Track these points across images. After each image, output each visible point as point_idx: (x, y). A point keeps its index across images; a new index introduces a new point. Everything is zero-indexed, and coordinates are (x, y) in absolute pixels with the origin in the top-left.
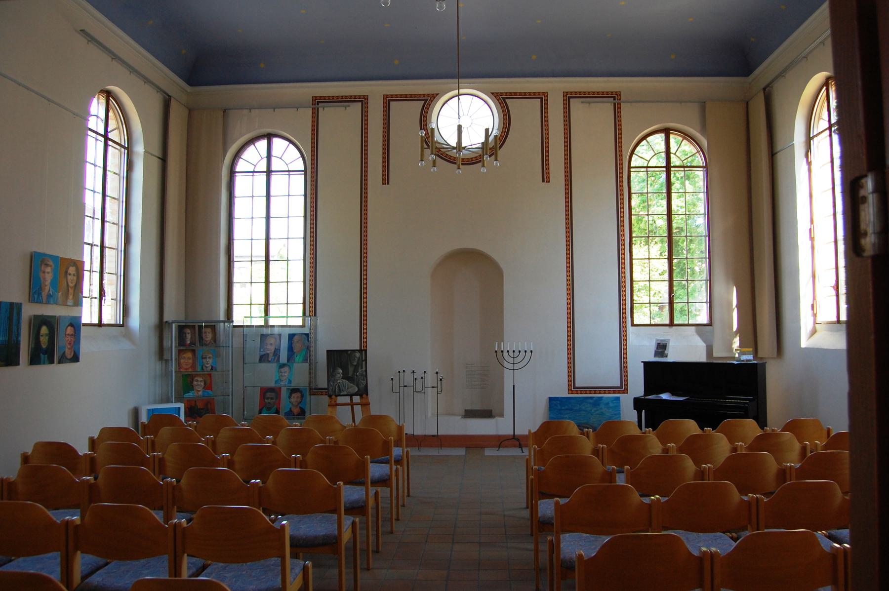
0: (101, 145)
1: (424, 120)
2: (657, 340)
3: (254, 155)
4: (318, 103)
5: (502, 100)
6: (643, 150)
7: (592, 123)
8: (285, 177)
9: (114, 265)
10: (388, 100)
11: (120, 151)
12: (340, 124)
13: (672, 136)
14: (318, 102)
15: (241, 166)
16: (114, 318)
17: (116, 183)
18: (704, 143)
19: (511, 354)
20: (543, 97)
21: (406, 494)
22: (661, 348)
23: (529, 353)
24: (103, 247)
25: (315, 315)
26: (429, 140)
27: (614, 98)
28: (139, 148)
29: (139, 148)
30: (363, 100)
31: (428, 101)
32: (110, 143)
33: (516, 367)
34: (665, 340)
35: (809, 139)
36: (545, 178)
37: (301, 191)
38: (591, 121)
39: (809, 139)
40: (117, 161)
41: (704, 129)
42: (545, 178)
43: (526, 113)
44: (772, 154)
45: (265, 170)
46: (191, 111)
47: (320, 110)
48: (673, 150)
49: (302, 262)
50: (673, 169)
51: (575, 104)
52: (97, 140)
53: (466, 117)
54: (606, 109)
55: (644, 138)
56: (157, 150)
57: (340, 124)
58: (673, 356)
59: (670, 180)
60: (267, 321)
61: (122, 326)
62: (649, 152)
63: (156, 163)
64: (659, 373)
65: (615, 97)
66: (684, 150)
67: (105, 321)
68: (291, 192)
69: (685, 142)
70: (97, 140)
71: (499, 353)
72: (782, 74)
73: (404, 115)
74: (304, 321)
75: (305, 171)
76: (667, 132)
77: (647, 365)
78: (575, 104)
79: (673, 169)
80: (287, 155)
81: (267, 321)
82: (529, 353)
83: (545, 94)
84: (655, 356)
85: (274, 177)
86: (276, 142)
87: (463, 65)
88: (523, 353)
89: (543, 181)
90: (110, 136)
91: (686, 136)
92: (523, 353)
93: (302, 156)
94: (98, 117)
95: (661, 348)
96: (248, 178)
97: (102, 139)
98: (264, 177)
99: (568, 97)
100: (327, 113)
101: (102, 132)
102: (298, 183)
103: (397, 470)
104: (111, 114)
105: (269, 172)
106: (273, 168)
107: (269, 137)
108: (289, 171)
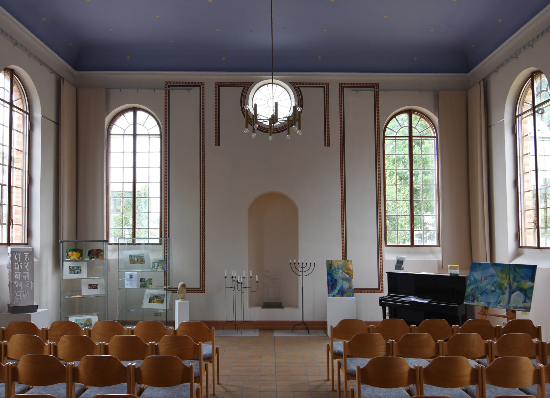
0: (8, 110)
1: (244, 101)
2: (397, 257)
3: (124, 123)
4: (169, 86)
5: (297, 89)
6: (393, 124)
7: (359, 104)
8: (146, 139)
9: (20, 200)
10: (219, 86)
11: (23, 115)
12: (185, 103)
13: (413, 116)
14: (169, 86)
15: (114, 130)
16: (20, 239)
17: (21, 140)
18: (436, 120)
19: (301, 265)
20: (325, 86)
21: (216, 382)
22: (400, 263)
23: (313, 265)
24: (10, 187)
25: (169, 237)
26: (251, 119)
27: (374, 88)
28: (38, 115)
29: (38, 115)
30: (200, 85)
31: (246, 88)
32: (15, 109)
33: (305, 274)
34: (402, 258)
35: (515, 117)
36: (327, 143)
37: (158, 149)
38: (359, 104)
39: (515, 117)
40: (21, 123)
41: (436, 111)
42: (327, 143)
43: (314, 96)
44: (488, 127)
45: (132, 133)
46: (77, 89)
47: (171, 91)
48: (413, 125)
49: (159, 199)
50: (413, 138)
51: (347, 91)
52: (4, 106)
53: (272, 99)
54: (369, 95)
55: (394, 116)
56: (53, 117)
57: (185, 103)
58: (407, 270)
59: (412, 148)
60: (134, 241)
61: (27, 244)
62: (398, 125)
63: (52, 126)
64: (399, 282)
65: (375, 87)
66: (421, 126)
67: (13, 241)
68: (151, 150)
69: (422, 119)
70: (4, 106)
71: (293, 265)
72: (496, 70)
73: (230, 96)
74: (161, 241)
75: (161, 135)
76: (410, 112)
77: (390, 274)
78: (347, 91)
79: (413, 138)
80: (148, 123)
81: (134, 241)
82: (313, 265)
83: (327, 84)
84: (396, 269)
85: (138, 139)
86: (140, 113)
87: (273, 64)
88: (308, 265)
89: (325, 146)
90: (15, 103)
91: (423, 115)
92: (308, 265)
93: (159, 124)
94: (4, 89)
95: (400, 263)
96: (120, 138)
97: (8, 106)
98: (131, 138)
99: (343, 86)
100: (175, 94)
101: (9, 101)
102: (156, 143)
103: (206, 366)
104: (15, 87)
105: (135, 135)
106: (138, 132)
107: (135, 110)
108: (149, 135)
